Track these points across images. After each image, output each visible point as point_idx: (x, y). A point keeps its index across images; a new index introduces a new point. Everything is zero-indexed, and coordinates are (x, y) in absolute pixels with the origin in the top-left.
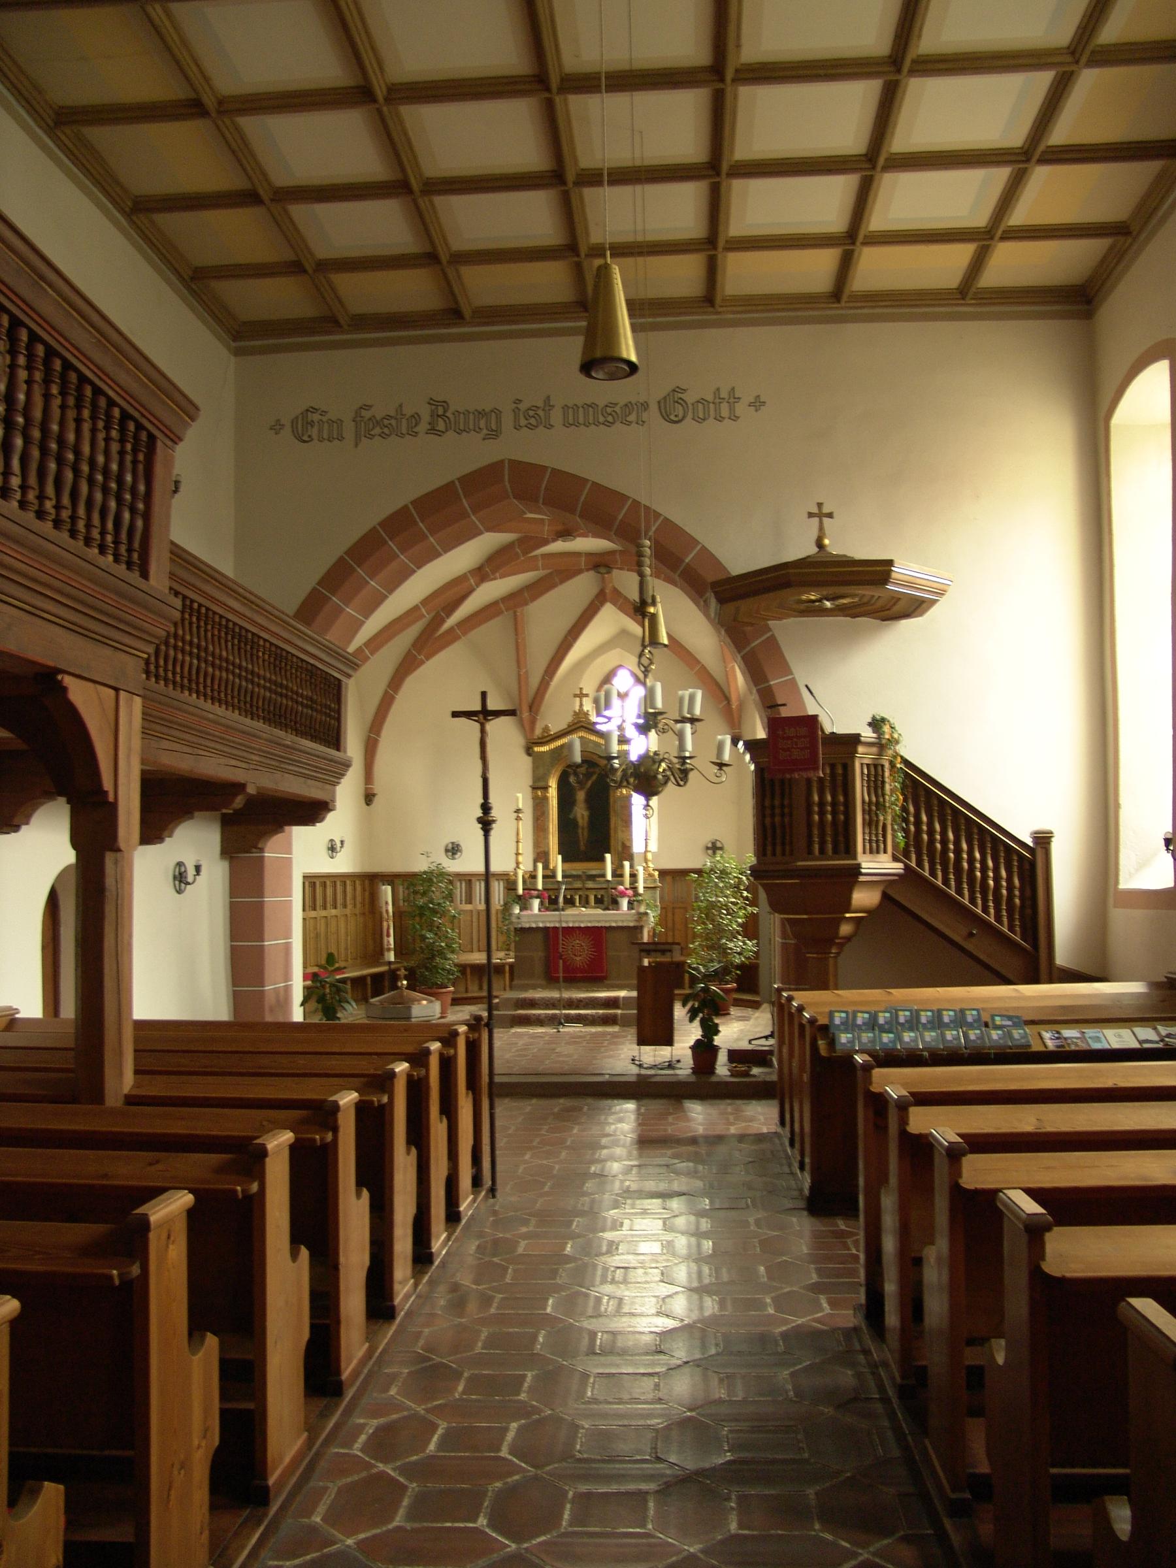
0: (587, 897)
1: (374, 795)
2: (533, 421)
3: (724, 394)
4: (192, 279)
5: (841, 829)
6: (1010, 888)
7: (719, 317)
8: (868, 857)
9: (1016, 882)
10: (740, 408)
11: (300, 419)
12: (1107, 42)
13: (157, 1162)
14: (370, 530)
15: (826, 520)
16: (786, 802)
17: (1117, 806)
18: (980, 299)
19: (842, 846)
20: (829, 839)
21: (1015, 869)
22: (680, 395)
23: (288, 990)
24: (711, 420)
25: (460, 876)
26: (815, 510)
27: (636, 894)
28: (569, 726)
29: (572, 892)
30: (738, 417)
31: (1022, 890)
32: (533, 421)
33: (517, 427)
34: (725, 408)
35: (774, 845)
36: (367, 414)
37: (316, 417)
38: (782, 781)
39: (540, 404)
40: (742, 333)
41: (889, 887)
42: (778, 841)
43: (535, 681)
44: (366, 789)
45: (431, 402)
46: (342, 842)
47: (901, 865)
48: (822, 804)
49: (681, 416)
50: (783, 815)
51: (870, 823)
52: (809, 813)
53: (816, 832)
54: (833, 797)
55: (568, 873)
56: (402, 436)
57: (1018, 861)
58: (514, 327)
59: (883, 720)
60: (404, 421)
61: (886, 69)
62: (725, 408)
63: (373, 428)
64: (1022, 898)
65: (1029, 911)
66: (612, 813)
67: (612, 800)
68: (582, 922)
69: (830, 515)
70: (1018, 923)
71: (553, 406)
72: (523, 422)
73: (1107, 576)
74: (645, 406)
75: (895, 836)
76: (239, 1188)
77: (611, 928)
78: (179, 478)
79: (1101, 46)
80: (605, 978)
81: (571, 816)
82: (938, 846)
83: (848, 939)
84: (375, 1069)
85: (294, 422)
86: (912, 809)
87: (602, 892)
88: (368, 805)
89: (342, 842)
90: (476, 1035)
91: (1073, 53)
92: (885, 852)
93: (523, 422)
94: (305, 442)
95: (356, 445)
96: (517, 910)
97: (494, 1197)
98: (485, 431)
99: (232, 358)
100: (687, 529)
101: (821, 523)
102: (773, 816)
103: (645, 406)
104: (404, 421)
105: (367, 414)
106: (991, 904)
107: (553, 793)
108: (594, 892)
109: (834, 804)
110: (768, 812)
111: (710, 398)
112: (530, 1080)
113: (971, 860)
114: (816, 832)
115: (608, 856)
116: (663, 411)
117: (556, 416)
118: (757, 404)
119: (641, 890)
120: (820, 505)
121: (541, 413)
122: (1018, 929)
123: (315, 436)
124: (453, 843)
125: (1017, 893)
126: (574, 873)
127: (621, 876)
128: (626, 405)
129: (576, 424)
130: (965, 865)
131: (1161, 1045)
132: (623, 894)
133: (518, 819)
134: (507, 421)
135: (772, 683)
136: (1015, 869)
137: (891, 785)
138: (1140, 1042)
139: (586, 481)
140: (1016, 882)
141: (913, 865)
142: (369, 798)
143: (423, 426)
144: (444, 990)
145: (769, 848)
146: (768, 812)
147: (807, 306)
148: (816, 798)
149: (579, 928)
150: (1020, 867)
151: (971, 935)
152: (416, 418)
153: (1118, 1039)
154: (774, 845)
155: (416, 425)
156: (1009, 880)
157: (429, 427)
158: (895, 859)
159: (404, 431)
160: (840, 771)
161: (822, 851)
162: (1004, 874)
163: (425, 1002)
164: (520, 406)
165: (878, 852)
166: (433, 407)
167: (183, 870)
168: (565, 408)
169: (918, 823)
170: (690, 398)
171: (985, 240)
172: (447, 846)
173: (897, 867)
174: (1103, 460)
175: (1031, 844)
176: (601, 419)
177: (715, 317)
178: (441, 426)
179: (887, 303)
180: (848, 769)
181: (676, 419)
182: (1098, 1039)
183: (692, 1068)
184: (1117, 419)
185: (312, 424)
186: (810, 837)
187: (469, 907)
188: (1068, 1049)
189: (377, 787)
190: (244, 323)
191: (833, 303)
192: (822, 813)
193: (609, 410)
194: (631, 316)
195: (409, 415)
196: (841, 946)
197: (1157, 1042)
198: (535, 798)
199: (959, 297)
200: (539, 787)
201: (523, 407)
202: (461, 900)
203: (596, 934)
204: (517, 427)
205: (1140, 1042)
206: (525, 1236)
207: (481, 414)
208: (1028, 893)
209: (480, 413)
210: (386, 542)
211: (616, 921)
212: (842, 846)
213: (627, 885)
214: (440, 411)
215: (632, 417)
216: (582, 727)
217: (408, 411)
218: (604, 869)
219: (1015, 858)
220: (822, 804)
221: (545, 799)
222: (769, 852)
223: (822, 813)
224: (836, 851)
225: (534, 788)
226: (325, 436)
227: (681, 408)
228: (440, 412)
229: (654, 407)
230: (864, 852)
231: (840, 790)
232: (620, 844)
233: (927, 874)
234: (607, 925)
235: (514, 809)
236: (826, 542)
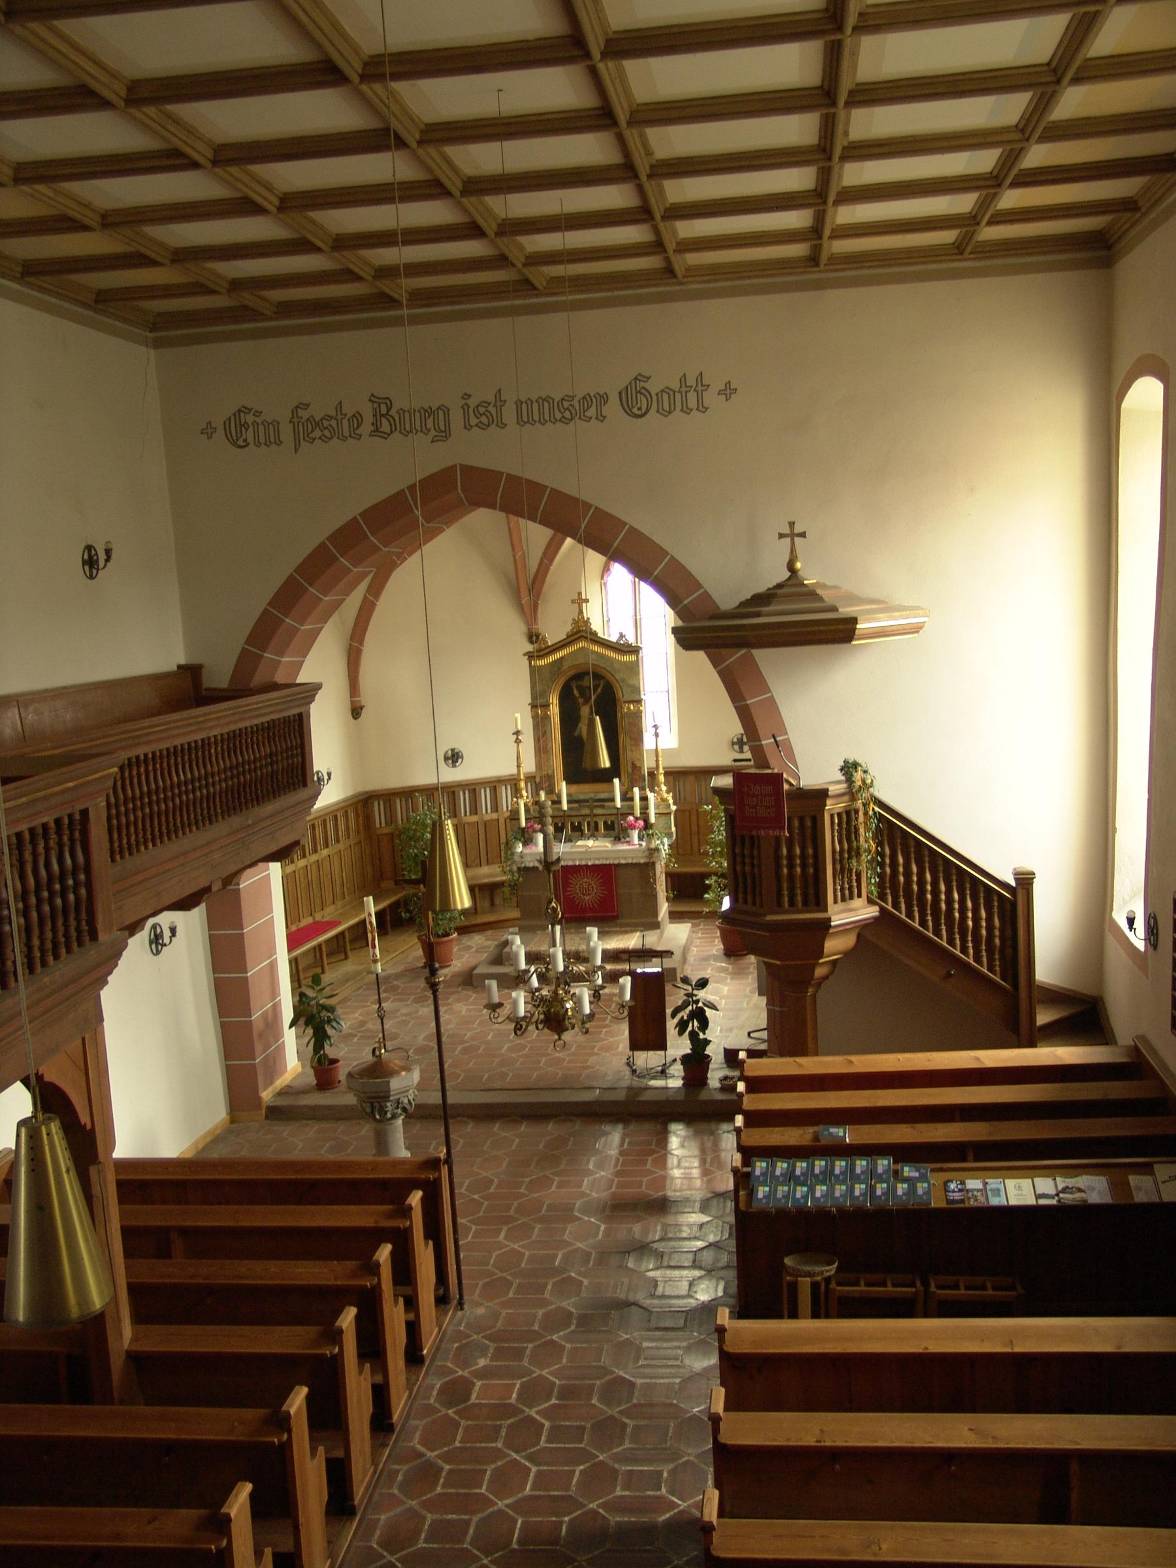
0: (596, 824)
1: (362, 708)
2: (484, 419)
3: (691, 381)
4: (96, 302)
5: (811, 881)
6: (990, 928)
7: (683, 287)
8: (840, 906)
9: (997, 922)
10: (710, 398)
11: (233, 418)
12: (1057, 119)
13: (155, 1519)
14: (320, 545)
15: (797, 540)
16: (755, 853)
17: (1115, 830)
18: (980, 252)
19: (812, 898)
20: (799, 892)
21: (996, 910)
22: (643, 384)
23: (276, 1009)
24: (677, 413)
25: (462, 785)
26: (787, 531)
27: (647, 825)
28: (568, 637)
29: (580, 819)
30: (707, 409)
31: (1002, 930)
32: (484, 419)
33: (467, 427)
34: (692, 398)
35: (745, 893)
36: (304, 414)
37: (250, 418)
38: (752, 838)
39: (492, 400)
40: (710, 306)
41: (863, 930)
42: (749, 890)
43: (533, 564)
44: (352, 702)
45: (373, 398)
46: (329, 774)
47: (876, 908)
48: (791, 857)
49: (644, 411)
50: (753, 865)
51: (842, 871)
52: (778, 867)
53: (785, 885)
54: (803, 849)
55: (575, 798)
56: (345, 439)
57: (998, 901)
58: (457, 307)
59: (855, 765)
60: (345, 422)
61: (817, 157)
62: (692, 398)
63: (312, 431)
64: (1002, 938)
65: (1009, 951)
66: (620, 730)
67: (619, 715)
68: (590, 860)
69: (803, 535)
70: (998, 963)
71: (505, 401)
72: (474, 421)
73: (1113, 579)
74: (604, 398)
75: (869, 882)
76: (213, 1547)
77: (619, 865)
78: (110, 546)
79: (1053, 122)
80: (616, 917)
81: (576, 734)
82: (915, 887)
83: (826, 978)
84: (336, 1279)
85: (226, 424)
86: (887, 851)
87: (613, 818)
88: (355, 718)
89: (329, 774)
90: (436, 1175)
91: (1022, 131)
92: (859, 896)
93: (474, 421)
94: (241, 447)
95: (296, 451)
96: (519, 848)
97: (462, 1309)
98: (433, 433)
99: (152, 352)
100: (654, 538)
101: (793, 544)
102: (744, 864)
103: (604, 398)
104: (345, 422)
105: (304, 414)
106: (970, 945)
107: (554, 709)
108: (603, 818)
109: (803, 856)
110: (739, 859)
111: (676, 387)
112: (523, 1100)
113: (950, 901)
114: (785, 885)
115: (616, 781)
116: (626, 407)
117: (509, 413)
118: (728, 391)
119: (652, 819)
120: (792, 524)
121: (492, 410)
122: (998, 968)
123: (250, 439)
124: (453, 750)
125: (997, 933)
126: (582, 797)
127: (632, 799)
128: (584, 398)
129: (531, 422)
130: (943, 906)
131: (1054, 1202)
132: (633, 827)
133: (518, 741)
134: (456, 418)
135: (748, 702)
136: (996, 910)
137: (866, 840)
138: (1038, 1197)
139: (545, 487)
140: (997, 922)
141: (890, 908)
142: (356, 711)
143: (367, 427)
144: (446, 939)
145: (741, 896)
146: (739, 859)
147: (782, 271)
148: (785, 851)
149: (587, 866)
150: (1001, 907)
151: (949, 975)
152: (358, 418)
153: (1016, 1192)
154: (745, 893)
155: (358, 427)
156: (989, 920)
157: (372, 428)
158: (871, 902)
159: (346, 433)
160: (809, 823)
161: (792, 903)
162: (983, 914)
163: (403, 1073)
164: (469, 402)
165: (851, 898)
166: (375, 405)
167: (159, 931)
168: (518, 404)
169: (894, 864)
170: (654, 387)
171: (969, 225)
172: (447, 752)
173: (872, 912)
174: (1114, 440)
175: (1013, 883)
176: (558, 416)
177: (678, 288)
178: (385, 427)
179: (874, 264)
180: (817, 821)
181: (639, 413)
182: (997, 1192)
183: (683, 1079)
184: (1124, 405)
185: (246, 426)
186: (780, 889)
187: (474, 818)
188: (967, 1205)
189: (366, 697)
190: (159, 314)
191: (812, 267)
192: (791, 866)
193: (566, 404)
194: (466, 865)
195: (349, 415)
196: (819, 985)
197: (1052, 1197)
198: (535, 717)
199: (956, 251)
200: (538, 705)
201: (472, 403)
202: (465, 812)
203: (605, 873)
204: (467, 427)
205: (1038, 1197)
206: (484, 1374)
207: (428, 412)
208: (1009, 932)
209: (426, 411)
210: (338, 559)
211: (625, 858)
212: (812, 898)
213: (638, 813)
214: (382, 406)
215: (592, 412)
216: (582, 636)
217: (349, 410)
218: (612, 791)
219: (995, 898)
220: (791, 857)
221: (546, 718)
222: (741, 901)
223: (791, 866)
224: (805, 903)
225: (534, 706)
226: (262, 440)
227: (644, 399)
228: (384, 410)
229: (614, 399)
230: (835, 902)
231: (809, 843)
232: (629, 763)
233: (903, 916)
234: (616, 862)
235: (514, 730)
236: (798, 565)
